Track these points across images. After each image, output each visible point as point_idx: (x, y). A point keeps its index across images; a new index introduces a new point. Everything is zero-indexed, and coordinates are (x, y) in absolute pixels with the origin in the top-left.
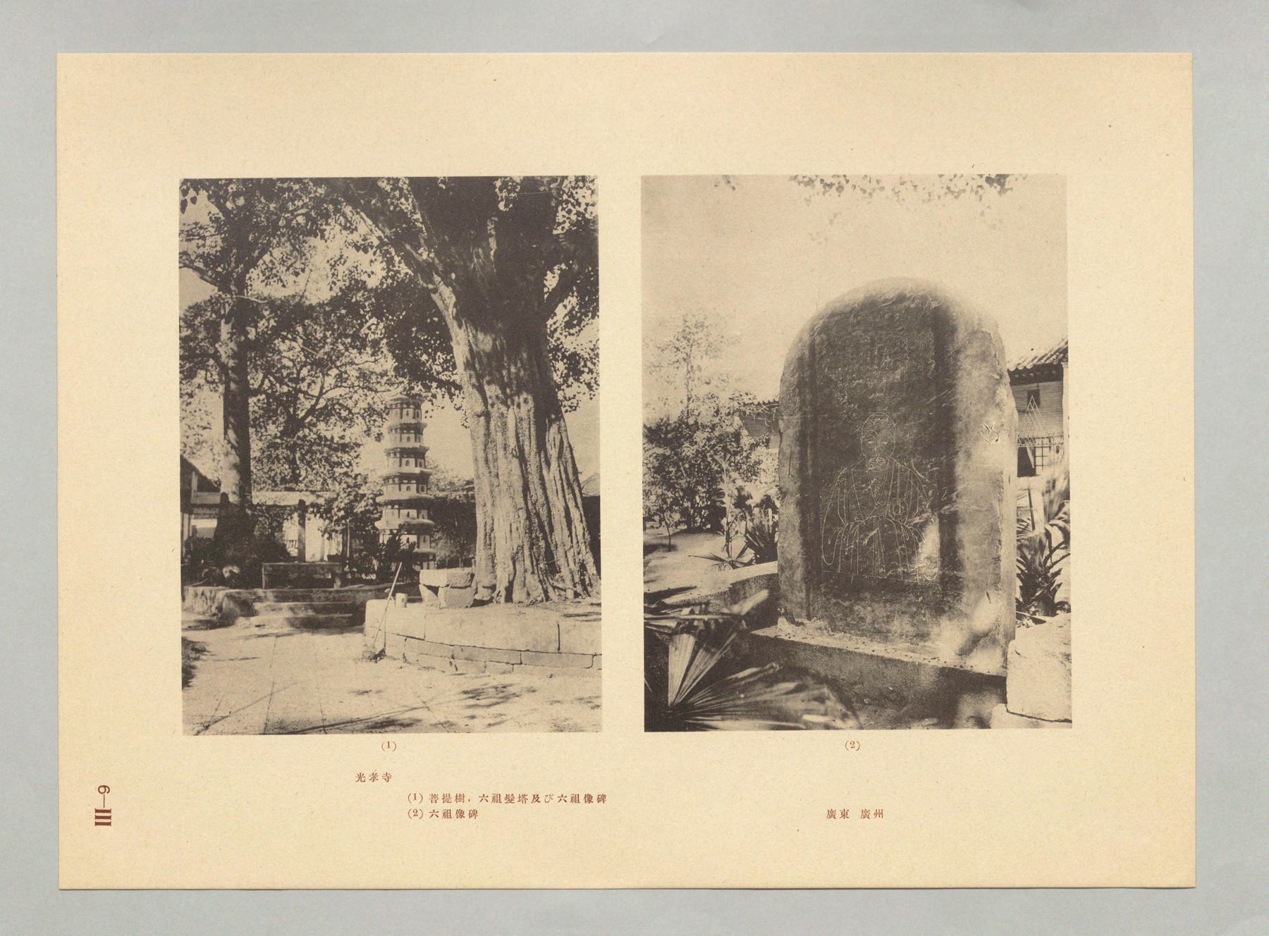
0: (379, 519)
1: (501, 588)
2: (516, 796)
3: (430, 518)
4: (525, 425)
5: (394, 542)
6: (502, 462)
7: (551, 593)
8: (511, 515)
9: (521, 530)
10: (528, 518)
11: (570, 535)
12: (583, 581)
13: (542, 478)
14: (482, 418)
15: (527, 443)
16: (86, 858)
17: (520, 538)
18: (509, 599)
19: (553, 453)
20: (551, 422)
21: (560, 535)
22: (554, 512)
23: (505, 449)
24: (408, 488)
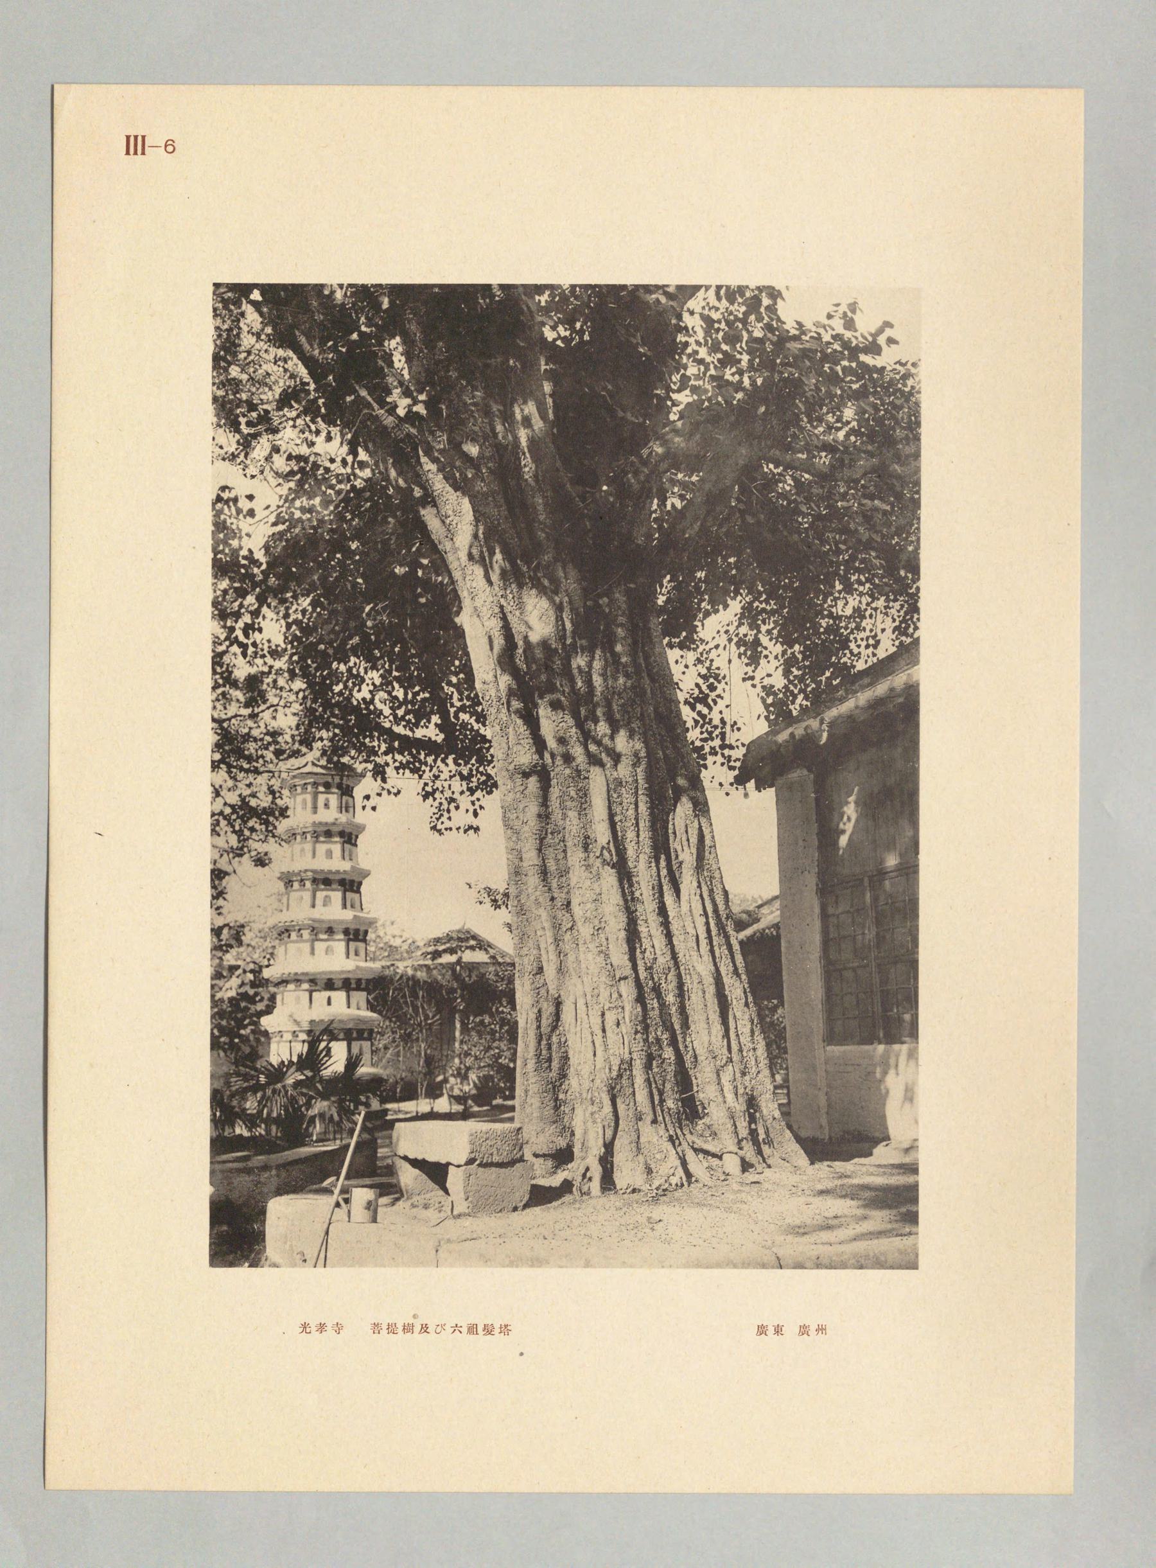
0: (269, 1010)
1: (588, 1158)
2: (813, 1328)
3: (371, 1007)
4: (627, 797)
5: (311, 1060)
6: (577, 875)
7: (697, 1165)
8: (604, 994)
9: (627, 1028)
10: (640, 999)
11: (727, 1034)
12: (753, 1133)
13: (662, 911)
14: (533, 782)
15: (630, 835)
16: (91, 115)
17: (622, 1043)
18: (608, 1182)
19: (687, 857)
20: (678, 793)
21: (704, 1035)
22: (690, 983)
23: (586, 848)
24: (328, 951)
